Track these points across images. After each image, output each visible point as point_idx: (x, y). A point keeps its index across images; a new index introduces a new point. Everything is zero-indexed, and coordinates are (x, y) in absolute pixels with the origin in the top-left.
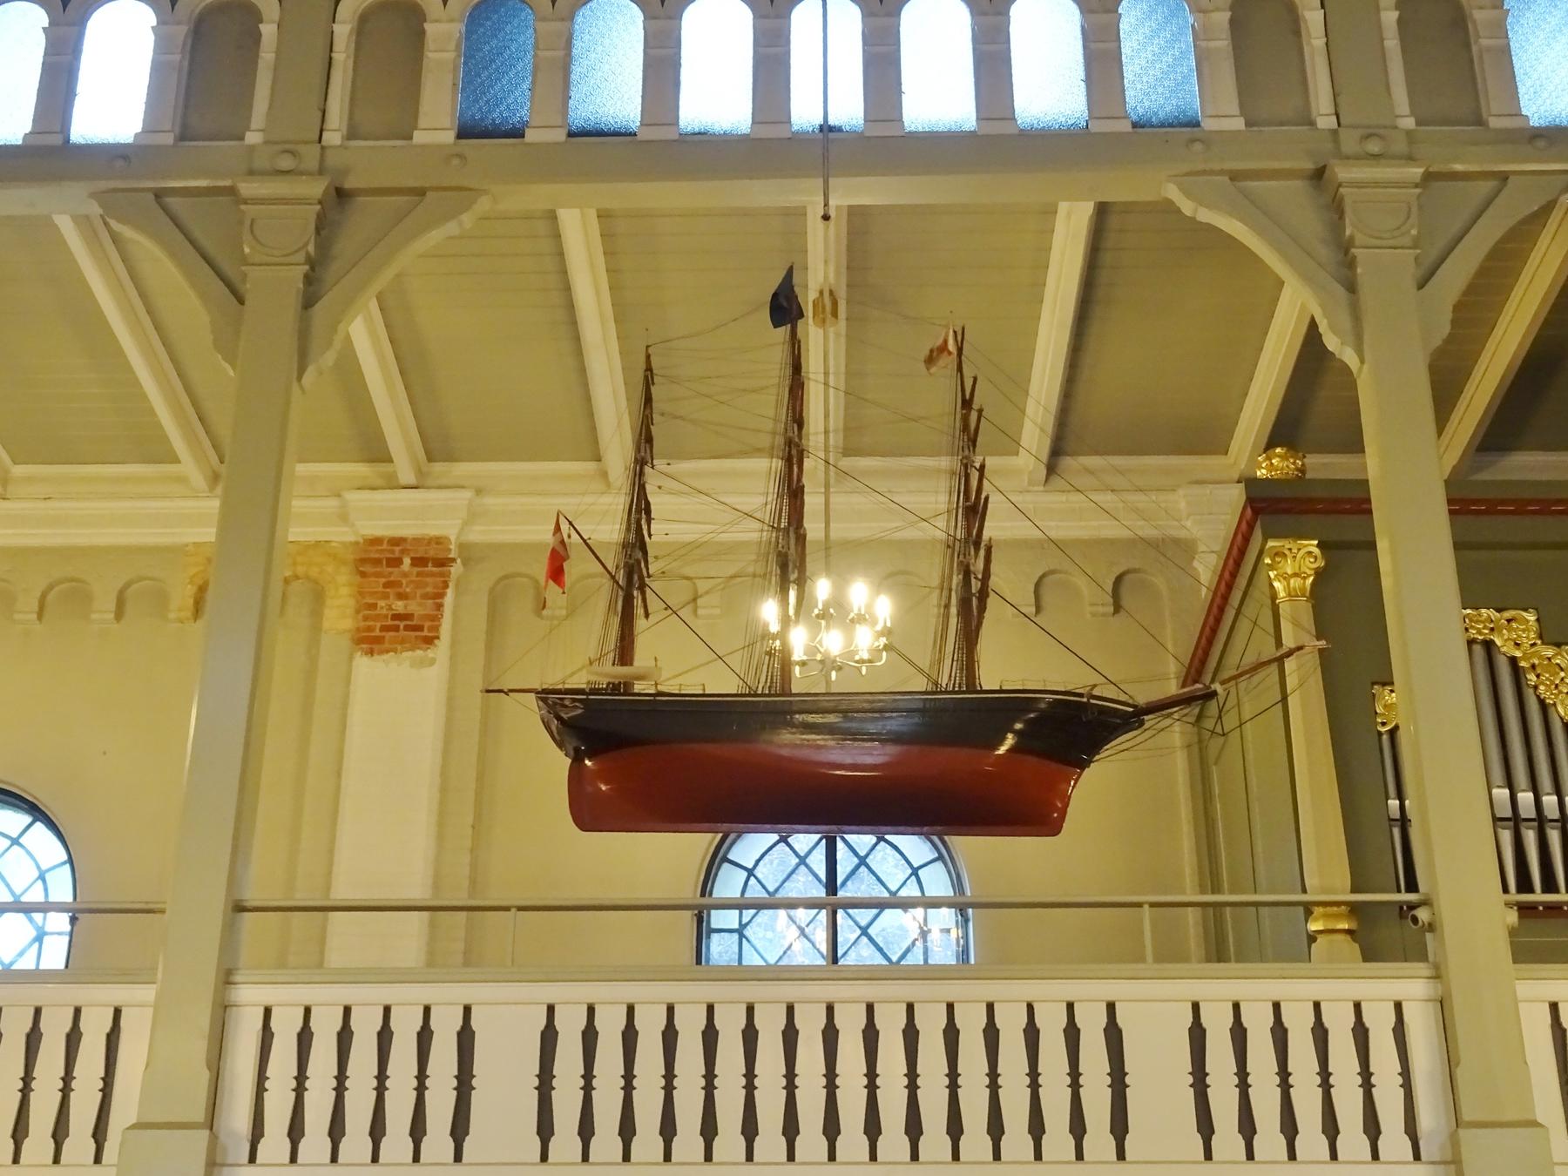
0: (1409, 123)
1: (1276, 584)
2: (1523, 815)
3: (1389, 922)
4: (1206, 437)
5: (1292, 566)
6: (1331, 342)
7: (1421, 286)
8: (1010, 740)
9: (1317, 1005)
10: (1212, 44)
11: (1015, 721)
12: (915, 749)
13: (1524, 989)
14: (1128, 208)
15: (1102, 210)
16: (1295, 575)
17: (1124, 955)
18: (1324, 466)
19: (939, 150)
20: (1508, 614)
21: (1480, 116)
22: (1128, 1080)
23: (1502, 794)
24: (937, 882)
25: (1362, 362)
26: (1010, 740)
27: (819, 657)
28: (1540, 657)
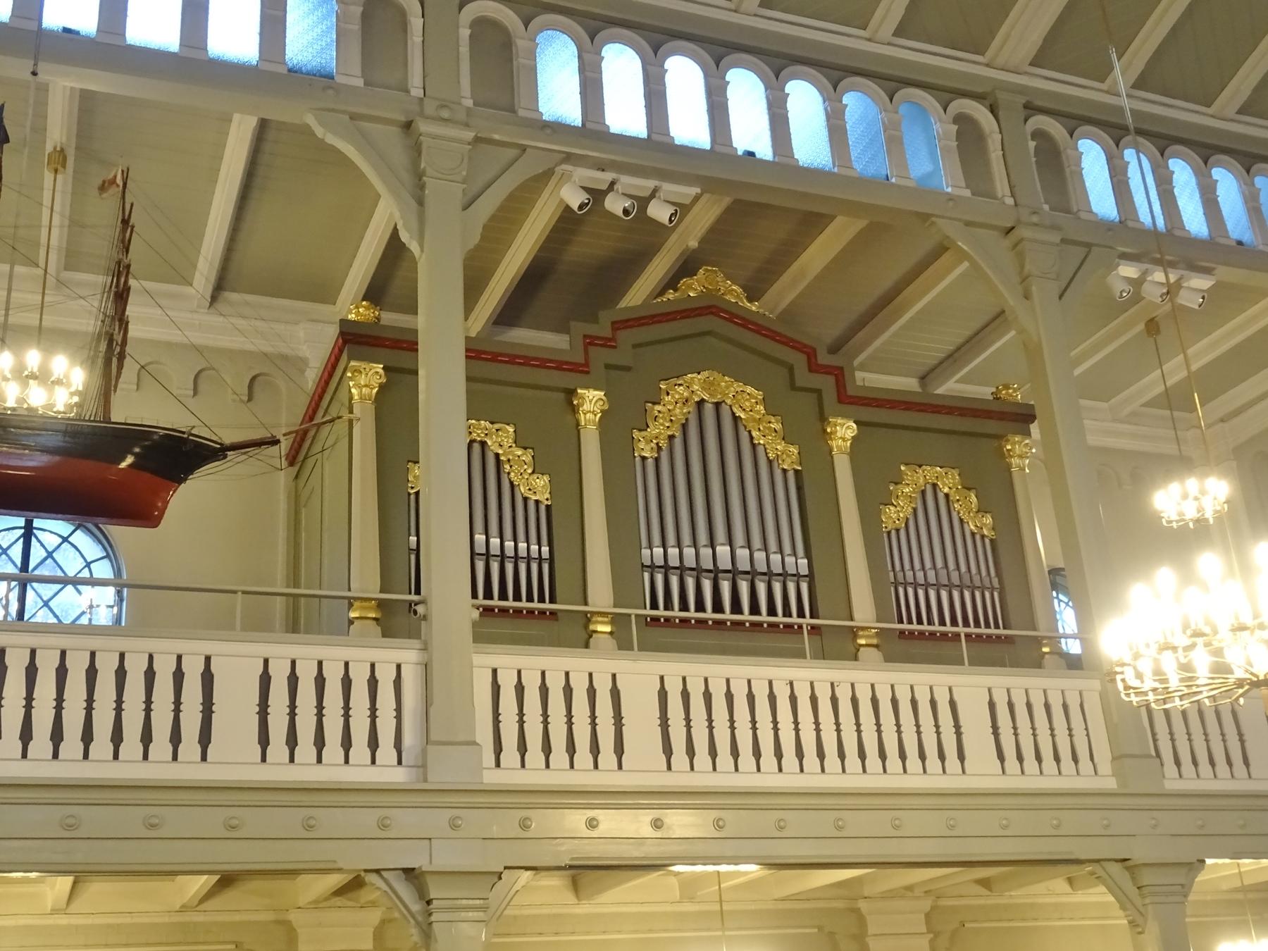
0: (469, 103)
1: (353, 390)
2: (492, 553)
3: (399, 616)
4: (324, 292)
5: (364, 380)
6: (404, 236)
7: (465, 208)
8: (130, 460)
9: (347, 664)
10: (350, 27)
11: (136, 445)
12: (57, 458)
13: (478, 659)
14: (282, 126)
15: (263, 125)
16: (366, 386)
17: (221, 626)
18: (390, 318)
19: (148, 61)
20: (497, 426)
21: (513, 105)
22: (214, 708)
23: (480, 538)
24: (103, 570)
25: (422, 251)
26: (130, 460)
27: (25, 406)
28: (514, 455)
